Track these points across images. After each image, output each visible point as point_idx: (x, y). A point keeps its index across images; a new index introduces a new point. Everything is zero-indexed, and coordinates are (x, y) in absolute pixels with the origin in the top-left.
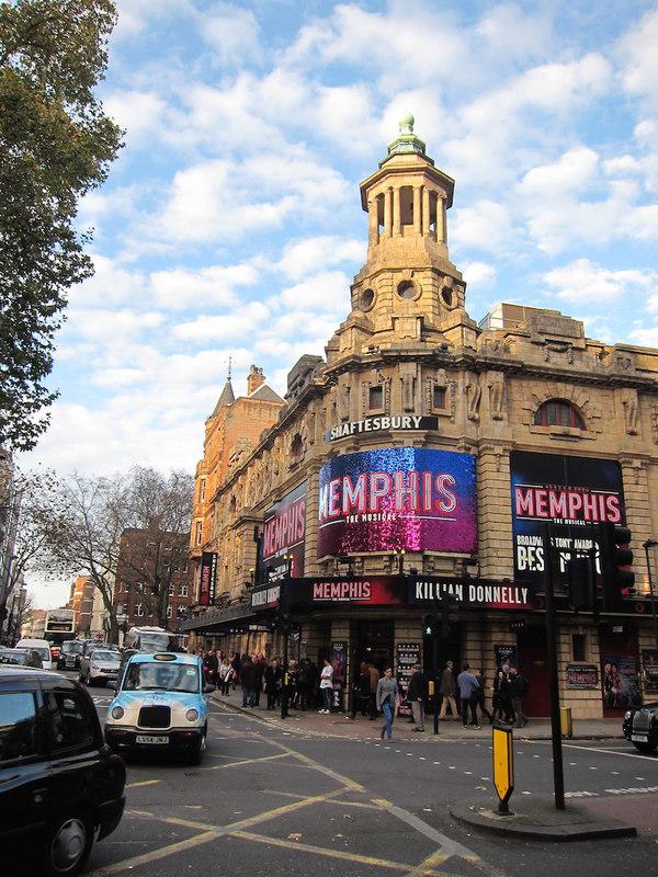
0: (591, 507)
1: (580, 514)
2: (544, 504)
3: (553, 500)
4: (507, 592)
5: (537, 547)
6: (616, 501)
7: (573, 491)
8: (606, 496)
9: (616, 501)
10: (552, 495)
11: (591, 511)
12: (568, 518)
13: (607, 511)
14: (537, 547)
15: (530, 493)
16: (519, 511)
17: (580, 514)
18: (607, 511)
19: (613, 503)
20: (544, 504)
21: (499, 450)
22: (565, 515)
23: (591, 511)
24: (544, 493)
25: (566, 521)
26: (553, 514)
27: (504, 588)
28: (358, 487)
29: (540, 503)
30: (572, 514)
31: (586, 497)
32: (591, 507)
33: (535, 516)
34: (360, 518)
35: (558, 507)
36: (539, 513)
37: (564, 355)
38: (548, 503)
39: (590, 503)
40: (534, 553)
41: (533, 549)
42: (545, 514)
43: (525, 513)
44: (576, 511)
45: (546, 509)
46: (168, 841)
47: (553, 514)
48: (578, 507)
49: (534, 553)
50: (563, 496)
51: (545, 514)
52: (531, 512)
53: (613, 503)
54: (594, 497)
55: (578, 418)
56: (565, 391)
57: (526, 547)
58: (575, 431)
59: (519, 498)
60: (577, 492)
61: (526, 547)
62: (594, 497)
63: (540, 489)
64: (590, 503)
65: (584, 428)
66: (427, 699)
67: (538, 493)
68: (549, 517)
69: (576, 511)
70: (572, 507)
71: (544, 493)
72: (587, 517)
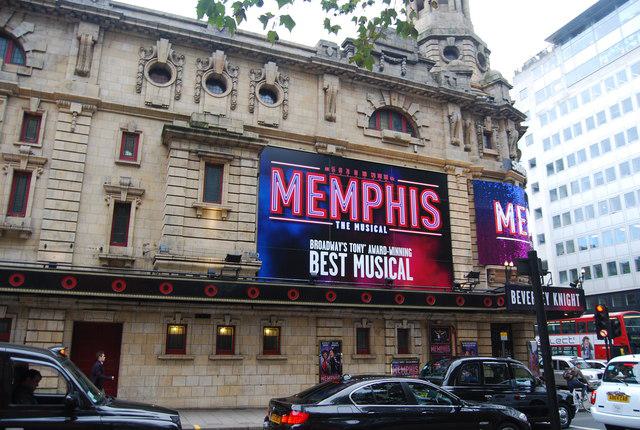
0: (395, 204)
1: (378, 215)
2: (320, 196)
3: (336, 191)
4: (530, 295)
5: (330, 252)
6: (435, 198)
7: (369, 178)
8: (420, 190)
9: (435, 198)
10: (335, 182)
11: (396, 211)
12: (360, 220)
13: (422, 212)
14: (330, 252)
15: (297, 177)
16: (275, 207)
17: (378, 215)
18: (422, 212)
19: (430, 200)
20: (320, 196)
21: (459, 171)
22: (354, 215)
23: (396, 211)
24: (322, 179)
25: (357, 226)
26: (334, 213)
27: (528, 292)
28: (508, 213)
29: (313, 195)
30: (366, 216)
31: (389, 189)
32: (395, 204)
33: (304, 215)
34: (352, 226)
35: (344, 203)
36: (311, 211)
37: (398, 67)
38: (328, 197)
39: (396, 198)
40: (327, 258)
41: (327, 254)
42: (321, 214)
43: (285, 209)
44: (373, 211)
45: (323, 204)
46: (97, 414)
47: (334, 213)
48: (377, 203)
49: (327, 258)
50: (353, 185)
51: (321, 214)
52: (297, 209)
53: (430, 200)
54: (401, 191)
55: (407, 123)
56: (398, 102)
57: (319, 251)
58: (405, 136)
59: (277, 184)
60: (376, 181)
61: (319, 251)
62: (401, 191)
63: (316, 172)
64: (396, 198)
65: (414, 135)
66: (574, 272)
67: (312, 180)
68: (328, 218)
69: (373, 211)
70: (367, 205)
71: (322, 179)
72: (390, 219)
